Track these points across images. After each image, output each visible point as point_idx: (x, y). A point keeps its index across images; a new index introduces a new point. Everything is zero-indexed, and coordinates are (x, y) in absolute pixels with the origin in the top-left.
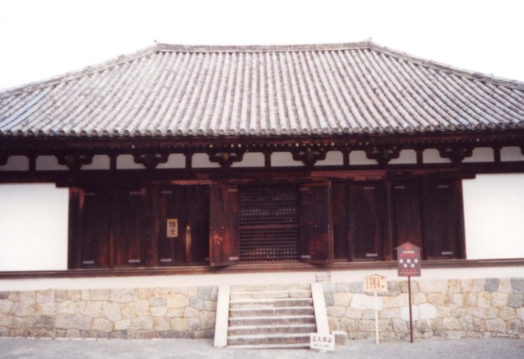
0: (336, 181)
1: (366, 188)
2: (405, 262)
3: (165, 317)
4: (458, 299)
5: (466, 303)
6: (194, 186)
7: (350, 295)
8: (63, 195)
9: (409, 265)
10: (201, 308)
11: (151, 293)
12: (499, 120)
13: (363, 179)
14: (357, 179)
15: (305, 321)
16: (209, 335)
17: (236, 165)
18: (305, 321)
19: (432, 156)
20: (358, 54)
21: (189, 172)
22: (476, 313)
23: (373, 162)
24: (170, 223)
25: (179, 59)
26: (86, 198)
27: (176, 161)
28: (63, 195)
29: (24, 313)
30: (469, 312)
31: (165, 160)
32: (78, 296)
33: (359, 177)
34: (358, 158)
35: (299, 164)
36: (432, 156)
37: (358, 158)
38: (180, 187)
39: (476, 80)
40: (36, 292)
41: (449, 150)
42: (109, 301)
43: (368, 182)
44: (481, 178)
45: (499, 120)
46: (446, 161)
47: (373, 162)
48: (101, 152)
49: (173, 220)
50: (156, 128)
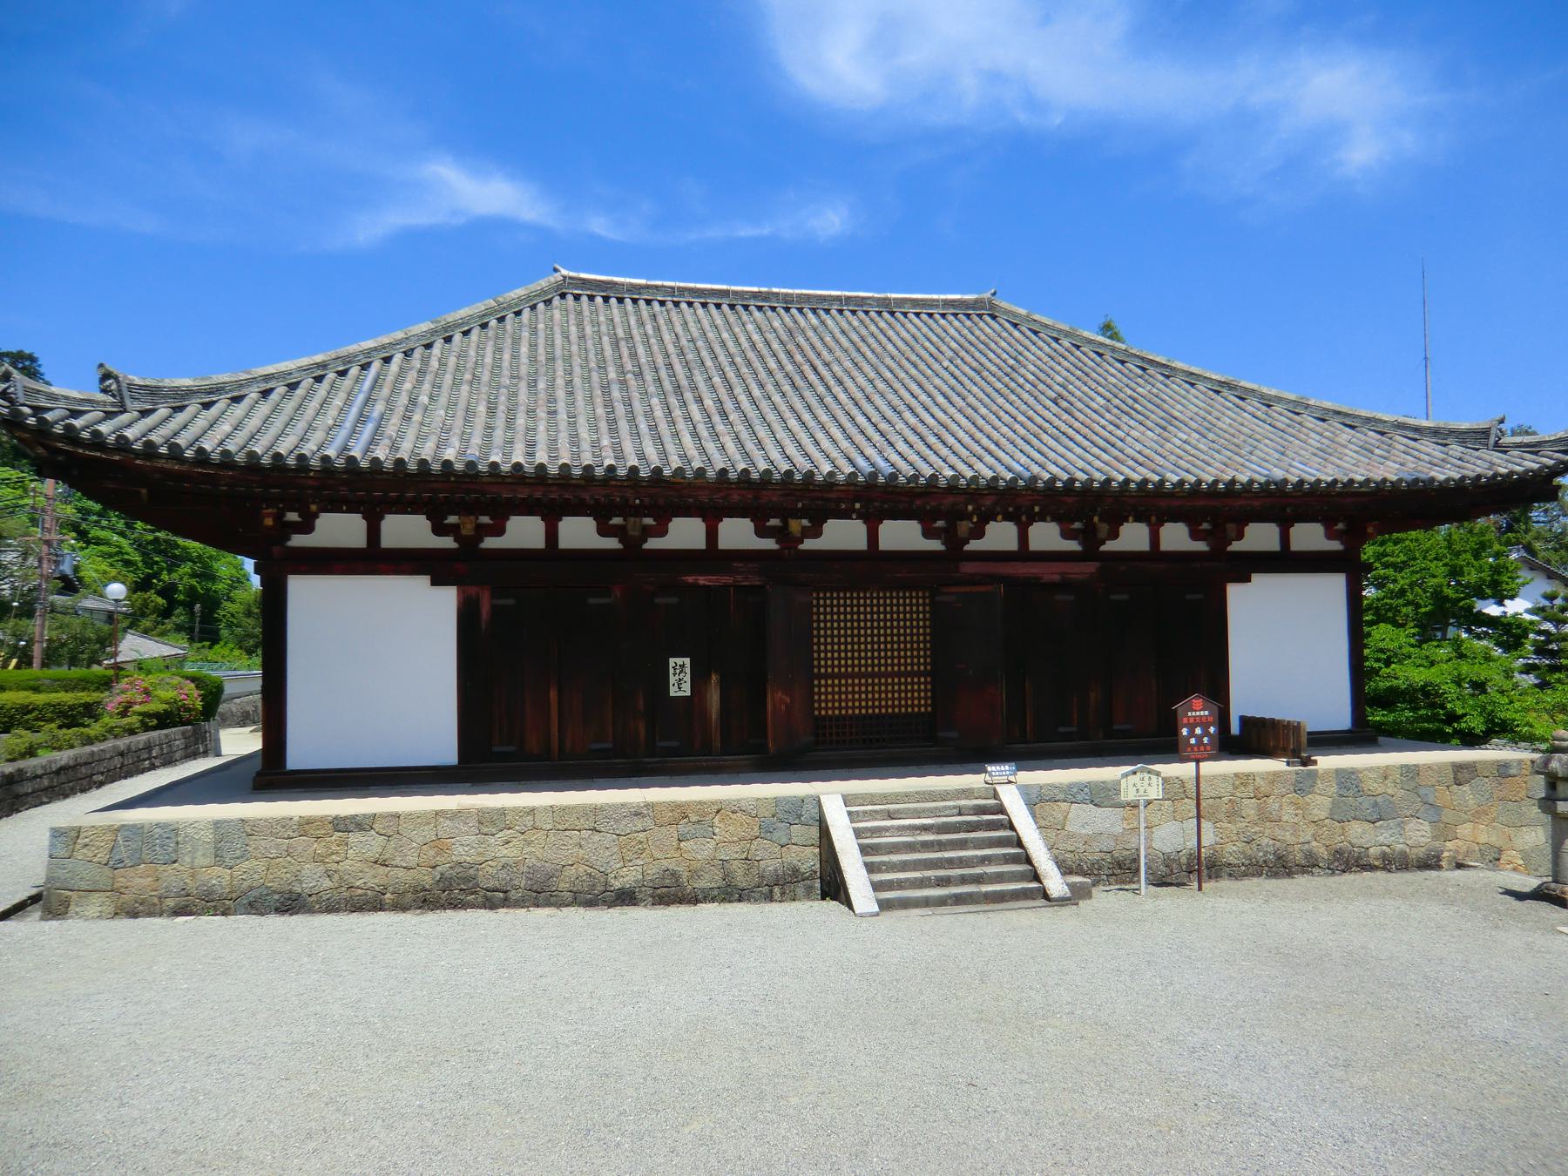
0: (1011, 582)
1: (1058, 597)
2: (1191, 733)
3: (710, 861)
4: (1250, 808)
5: (1264, 817)
6: (726, 587)
7: (1064, 805)
8: (446, 600)
9: (1199, 738)
10: (784, 840)
11: (681, 812)
12: (873, 465)
13: (1057, 578)
14: (1046, 578)
15: (1009, 859)
16: (833, 887)
17: (653, 543)
18: (1009, 859)
19: (1176, 537)
20: (804, 315)
21: (712, 557)
22: (1278, 833)
23: (1073, 546)
24: (682, 666)
25: (557, 314)
26: (495, 610)
27: (685, 533)
28: (446, 600)
29: (412, 860)
30: (1267, 832)
31: (662, 531)
32: (529, 821)
33: (1050, 573)
34: (1046, 536)
35: (936, 545)
36: (1176, 537)
37: (1046, 536)
38: (696, 586)
39: (1225, 392)
40: (437, 813)
41: (940, 523)
42: (594, 829)
43: (1064, 585)
44: (1262, 583)
45: (873, 465)
46: (1201, 546)
47: (1073, 546)
48: (527, 509)
49: (679, 661)
50: (367, 450)
